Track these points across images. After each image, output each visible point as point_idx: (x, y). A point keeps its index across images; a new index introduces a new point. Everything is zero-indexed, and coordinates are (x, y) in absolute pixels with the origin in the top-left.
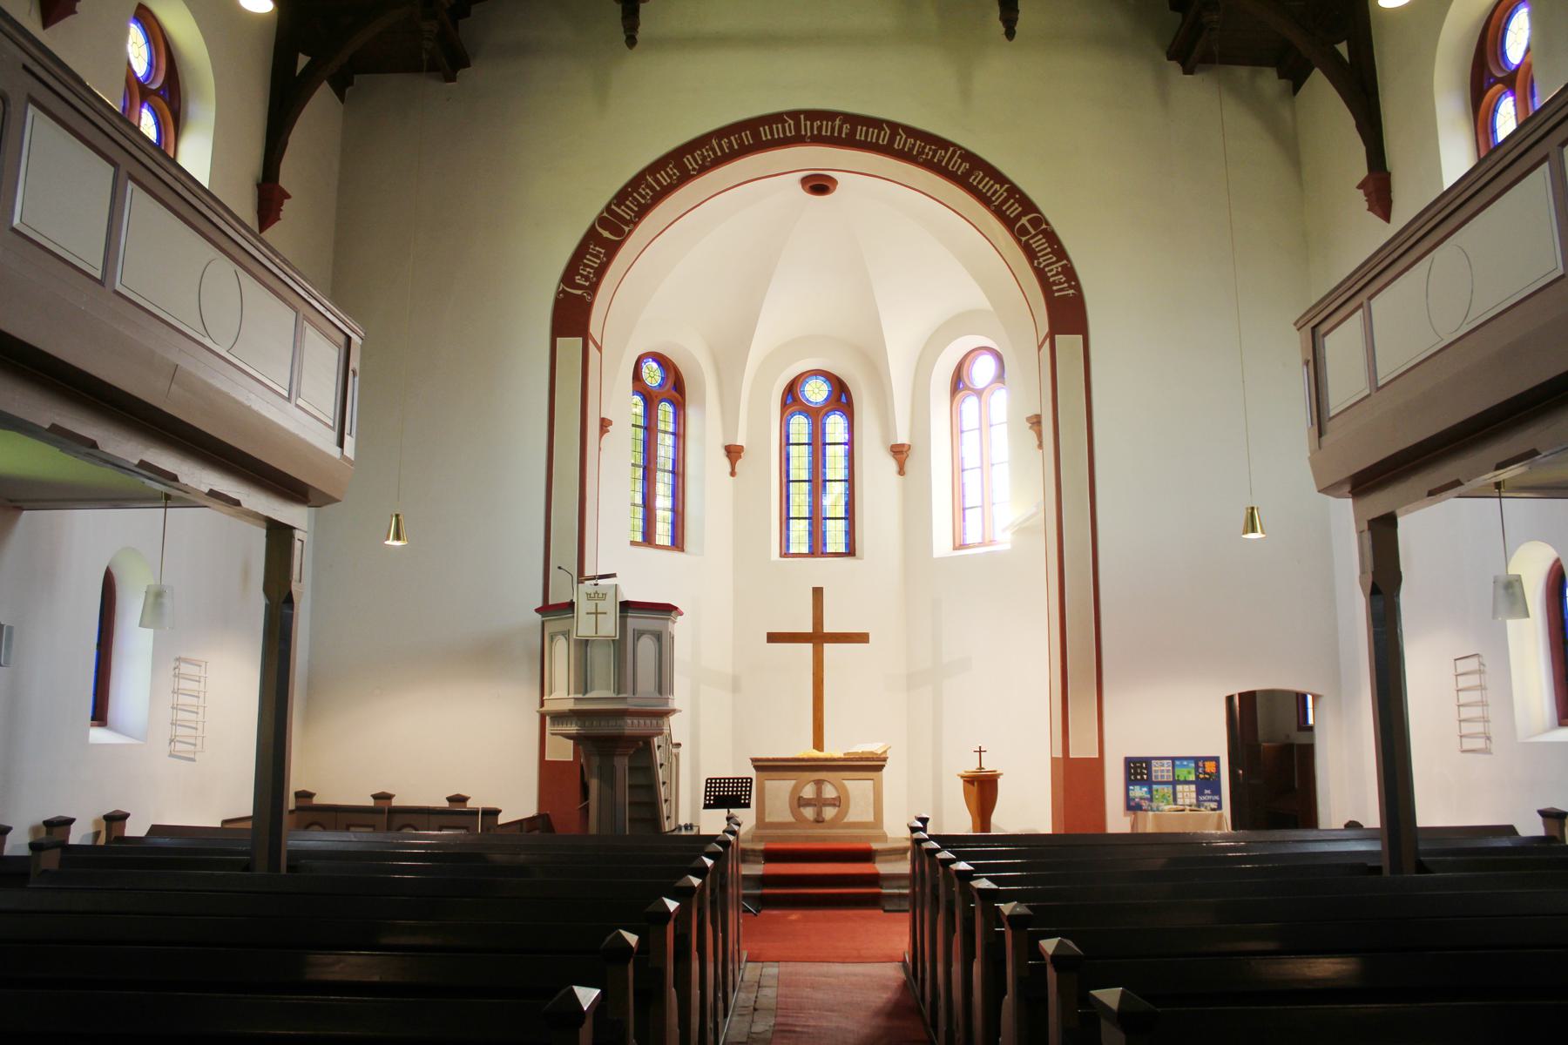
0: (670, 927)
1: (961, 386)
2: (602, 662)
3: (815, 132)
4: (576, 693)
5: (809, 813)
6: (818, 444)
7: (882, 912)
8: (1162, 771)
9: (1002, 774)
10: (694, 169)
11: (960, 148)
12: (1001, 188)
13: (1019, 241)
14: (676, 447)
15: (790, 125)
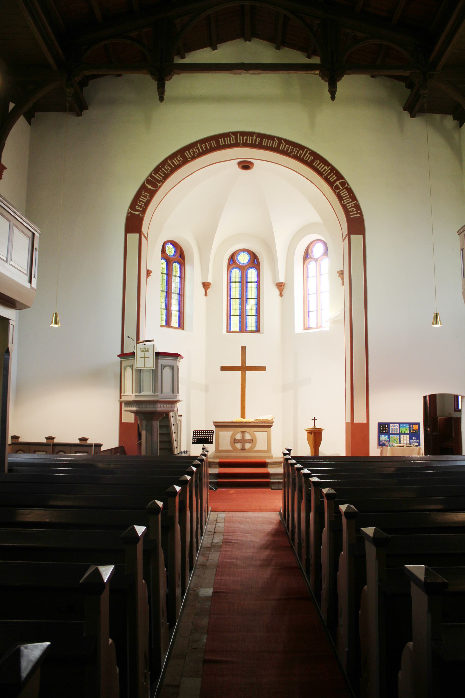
1: (308, 257)
2: (147, 379)
3: (244, 142)
4: (136, 392)
5: (239, 446)
6: (244, 282)
7: (271, 489)
8: (395, 429)
9: (324, 430)
10: (189, 158)
11: (309, 150)
12: (327, 168)
13: (335, 192)
14: (180, 283)
15: (233, 138)
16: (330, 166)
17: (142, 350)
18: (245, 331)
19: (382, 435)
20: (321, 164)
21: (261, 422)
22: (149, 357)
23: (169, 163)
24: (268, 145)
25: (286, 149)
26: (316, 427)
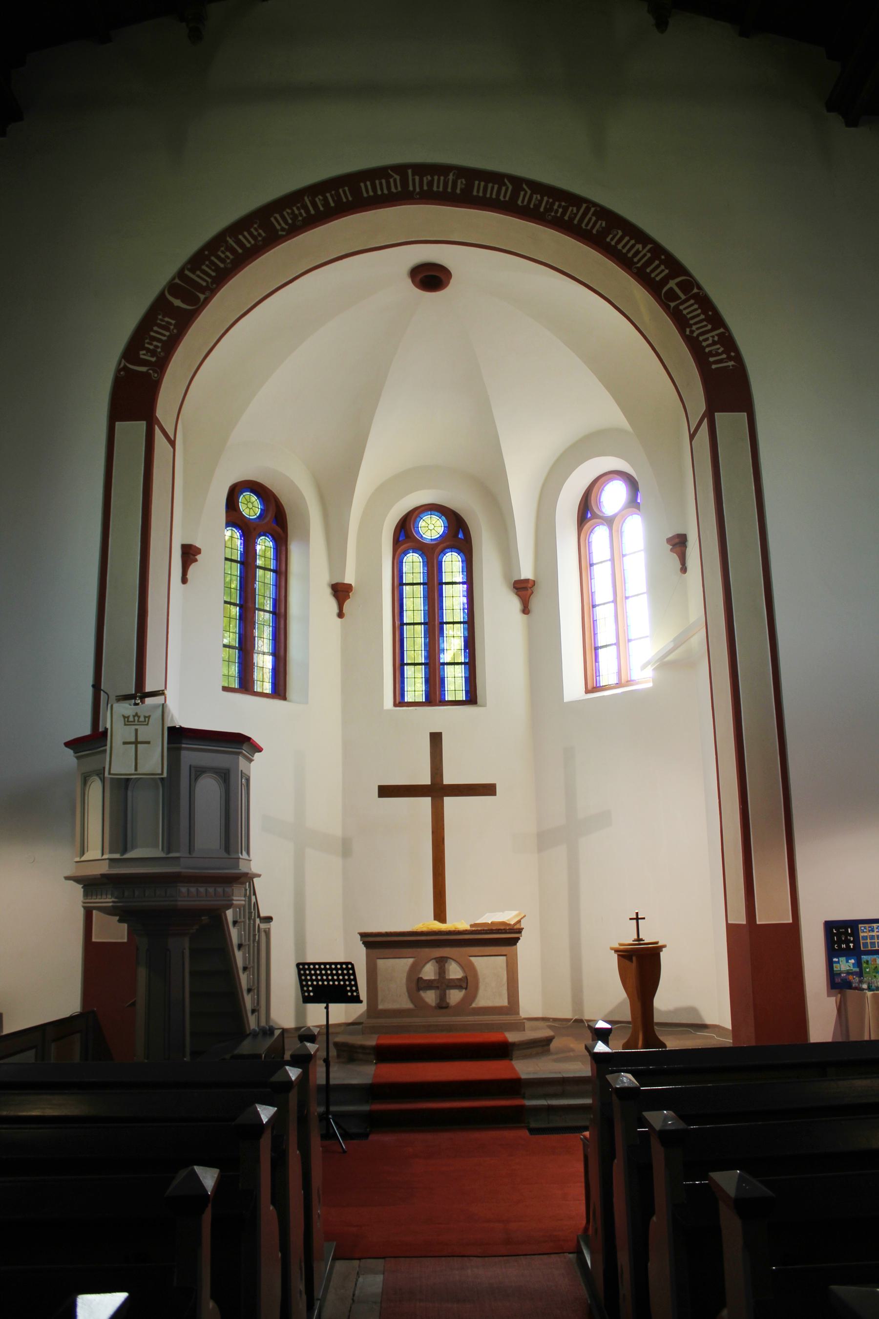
0: (266, 1142)
1: (589, 515)
3: (425, 188)
4: (111, 852)
5: (430, 997)
7: (525, 1133)
8: (872, 937)
9: (664, 946)
10: (283, 229)
11: (595, 205)
12: (644, 248)
15: (395, 181)
16: (651, 244)
17: (128, 721)
18: (440, 702)
19: (838, 957)
20: (627, 238)
21: (488, 930)
22: (148, 743)
23: (230, 244)
24: (488, 195)
25: (535, 205)
26: (642, 940)
